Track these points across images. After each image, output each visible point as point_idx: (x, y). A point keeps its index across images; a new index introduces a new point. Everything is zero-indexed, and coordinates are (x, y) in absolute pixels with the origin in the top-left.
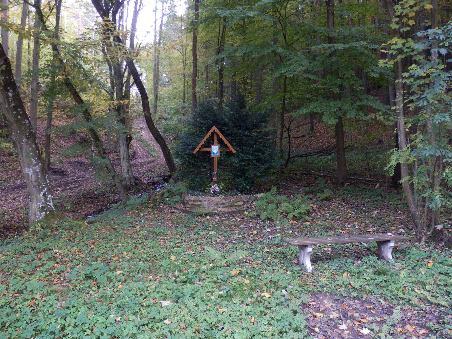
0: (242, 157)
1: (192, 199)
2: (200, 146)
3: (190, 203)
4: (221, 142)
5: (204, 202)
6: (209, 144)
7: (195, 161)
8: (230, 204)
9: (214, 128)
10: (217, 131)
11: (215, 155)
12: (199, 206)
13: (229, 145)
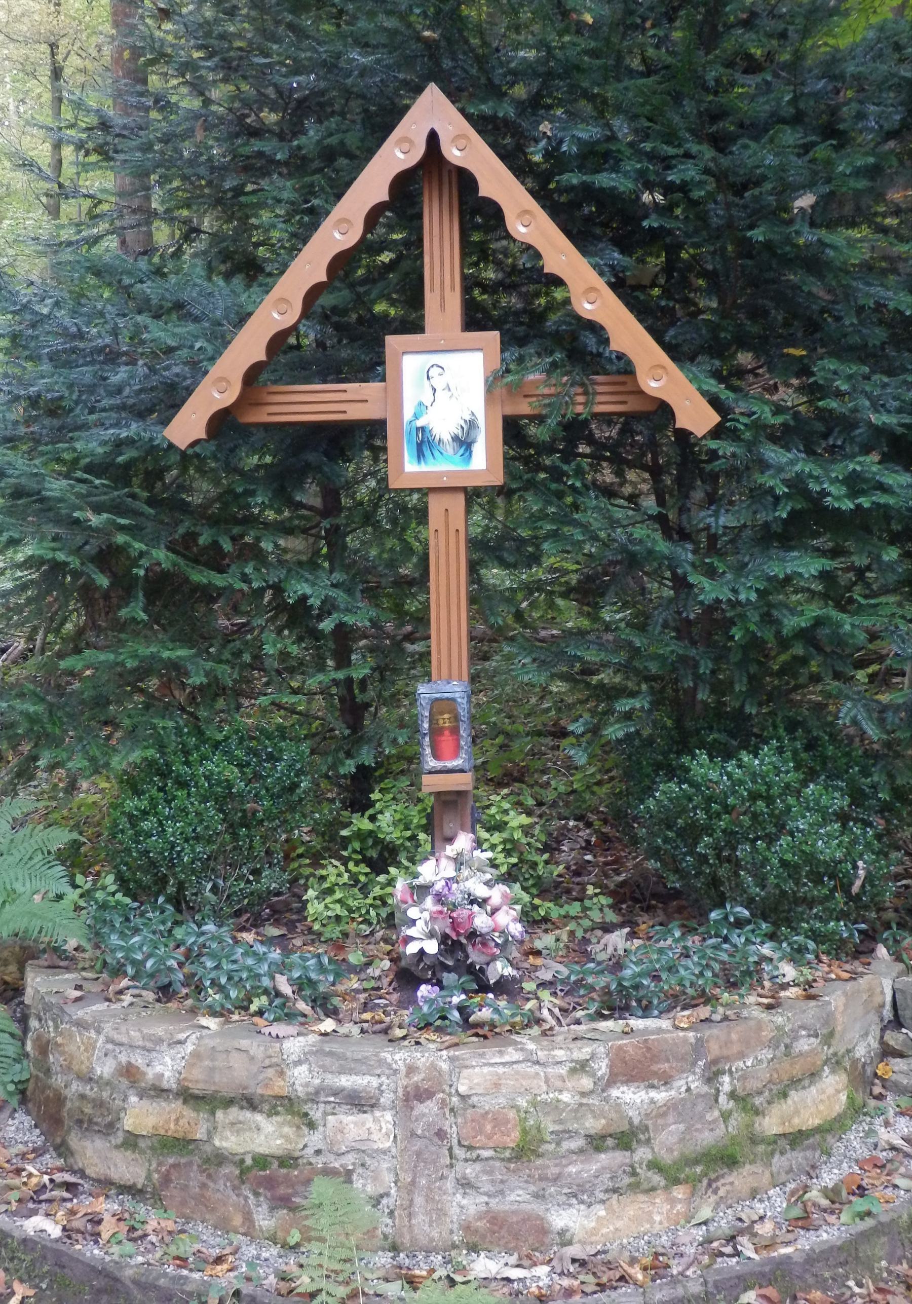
0: (797, 485)
1: (166, 1067)
2: (248, 347)
3: (140, 1116)
4: (514, 309)
5: (351, 1126)
6: (360, 321)
7: (184, 547)
8: (707, 1138)
9: (433, 115)
10: (468, 150)
11: (443, 466)
12: (276, 1179)
13: (627, 334)
